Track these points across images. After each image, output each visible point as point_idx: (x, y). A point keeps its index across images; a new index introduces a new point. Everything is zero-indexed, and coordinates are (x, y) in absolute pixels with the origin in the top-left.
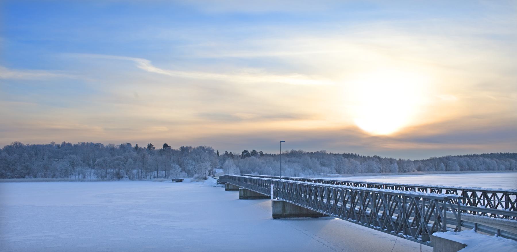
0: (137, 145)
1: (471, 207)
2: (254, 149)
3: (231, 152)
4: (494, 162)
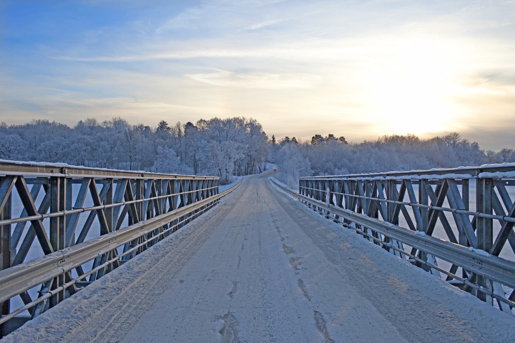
0: (168, 124)
1: (428, 193)
2: (286, 136)
3: (294, 138)
4: (44, 169)
